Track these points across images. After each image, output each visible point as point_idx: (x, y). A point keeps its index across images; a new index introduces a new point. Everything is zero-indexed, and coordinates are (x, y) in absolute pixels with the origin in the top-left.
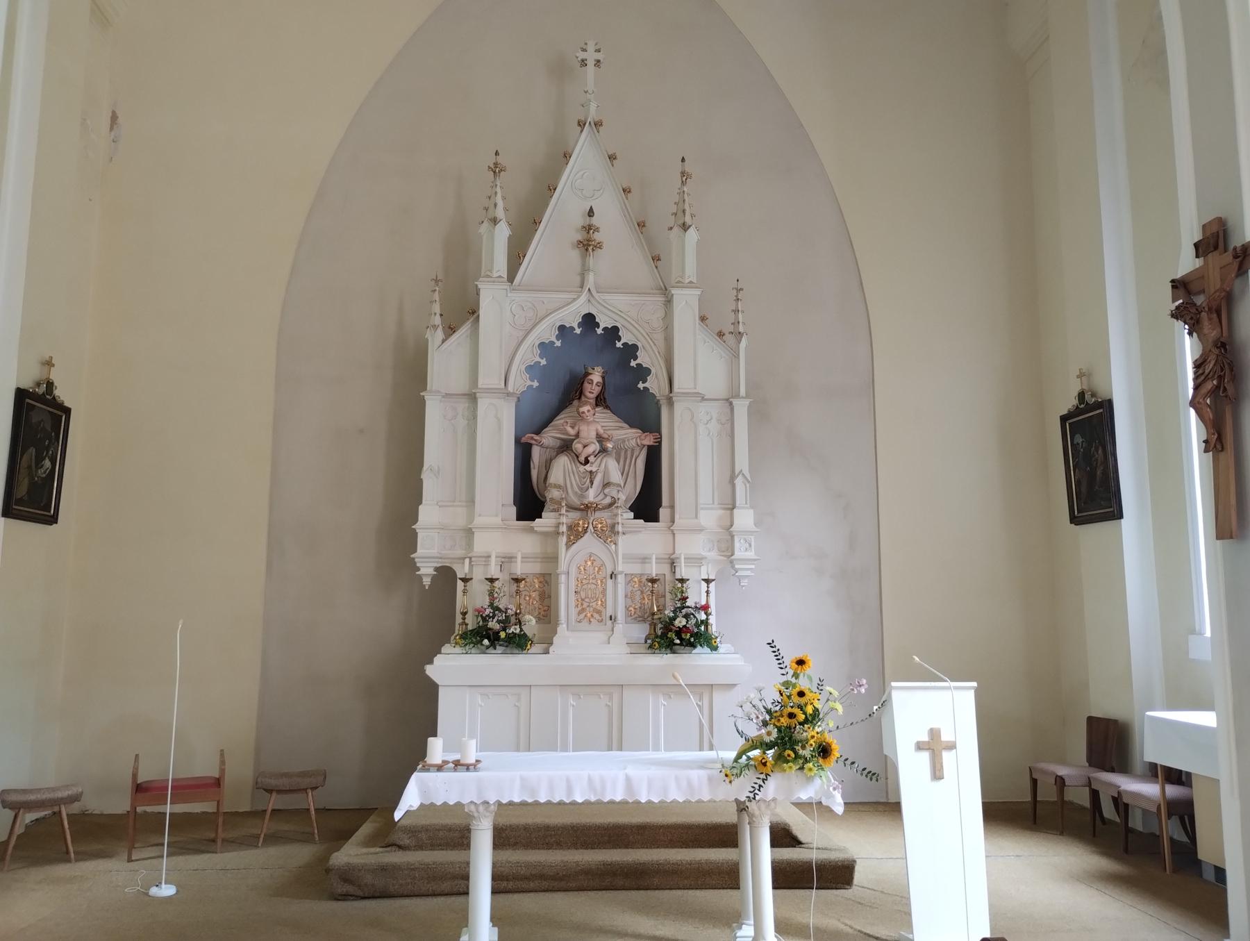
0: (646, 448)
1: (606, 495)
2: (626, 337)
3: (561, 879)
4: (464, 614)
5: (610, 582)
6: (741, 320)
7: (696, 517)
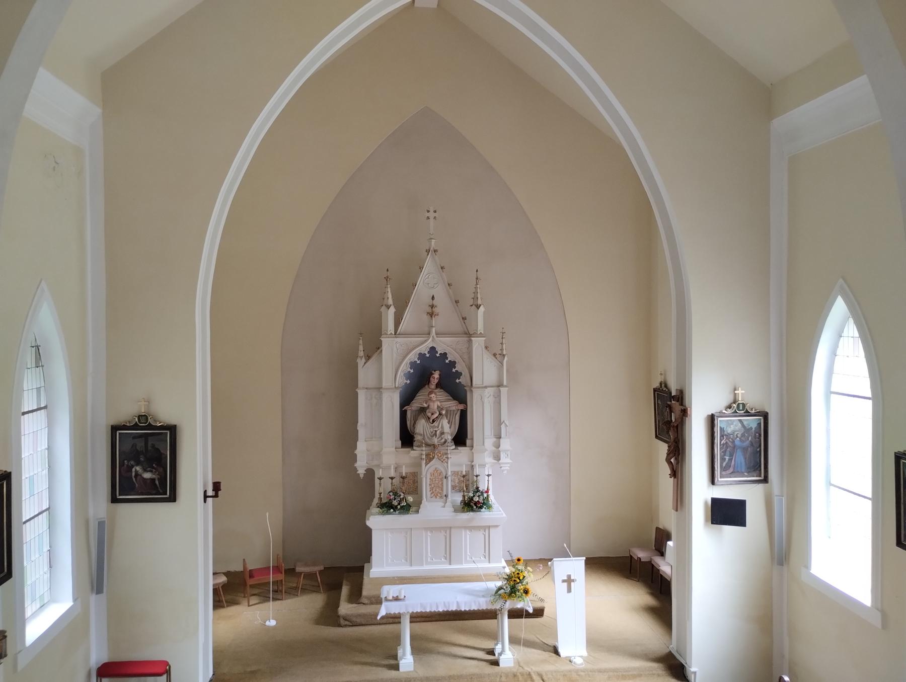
0: (459, 411)
1: (442, 439)
2: (450, 358)
3: (429, 617)
4: (380, 494)
5: (445, 480)
6: (504, 348)
7: (483, 445)
